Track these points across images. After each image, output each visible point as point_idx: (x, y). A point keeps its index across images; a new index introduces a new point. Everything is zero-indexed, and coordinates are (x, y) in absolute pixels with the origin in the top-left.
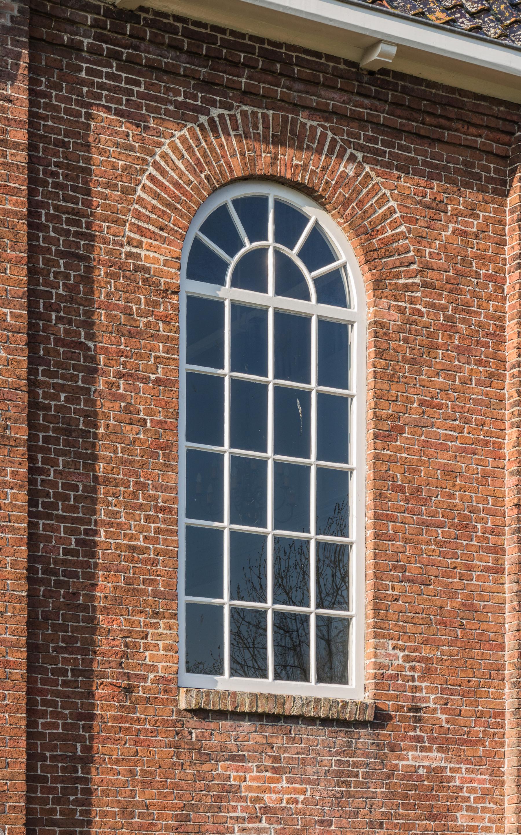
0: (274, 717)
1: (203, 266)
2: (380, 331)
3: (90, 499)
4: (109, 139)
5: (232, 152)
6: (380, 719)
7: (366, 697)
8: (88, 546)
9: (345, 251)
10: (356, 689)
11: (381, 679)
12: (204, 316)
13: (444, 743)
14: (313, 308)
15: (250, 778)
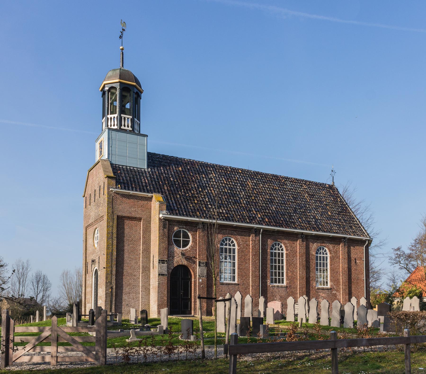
0: (323, 289)
1: (317, 253)
2: (330, 257)
3: (310, 273)
4: (311, 244)
5: (319, 244)
6: (331, 289)
7: (330, 287)
8: (310, 276)
9: (235, 242)
10: (329, 286)
11: (331, 286)
12: (272, 253)
13: (336, 291)
14: (232, 247)
15: (321, 294)
